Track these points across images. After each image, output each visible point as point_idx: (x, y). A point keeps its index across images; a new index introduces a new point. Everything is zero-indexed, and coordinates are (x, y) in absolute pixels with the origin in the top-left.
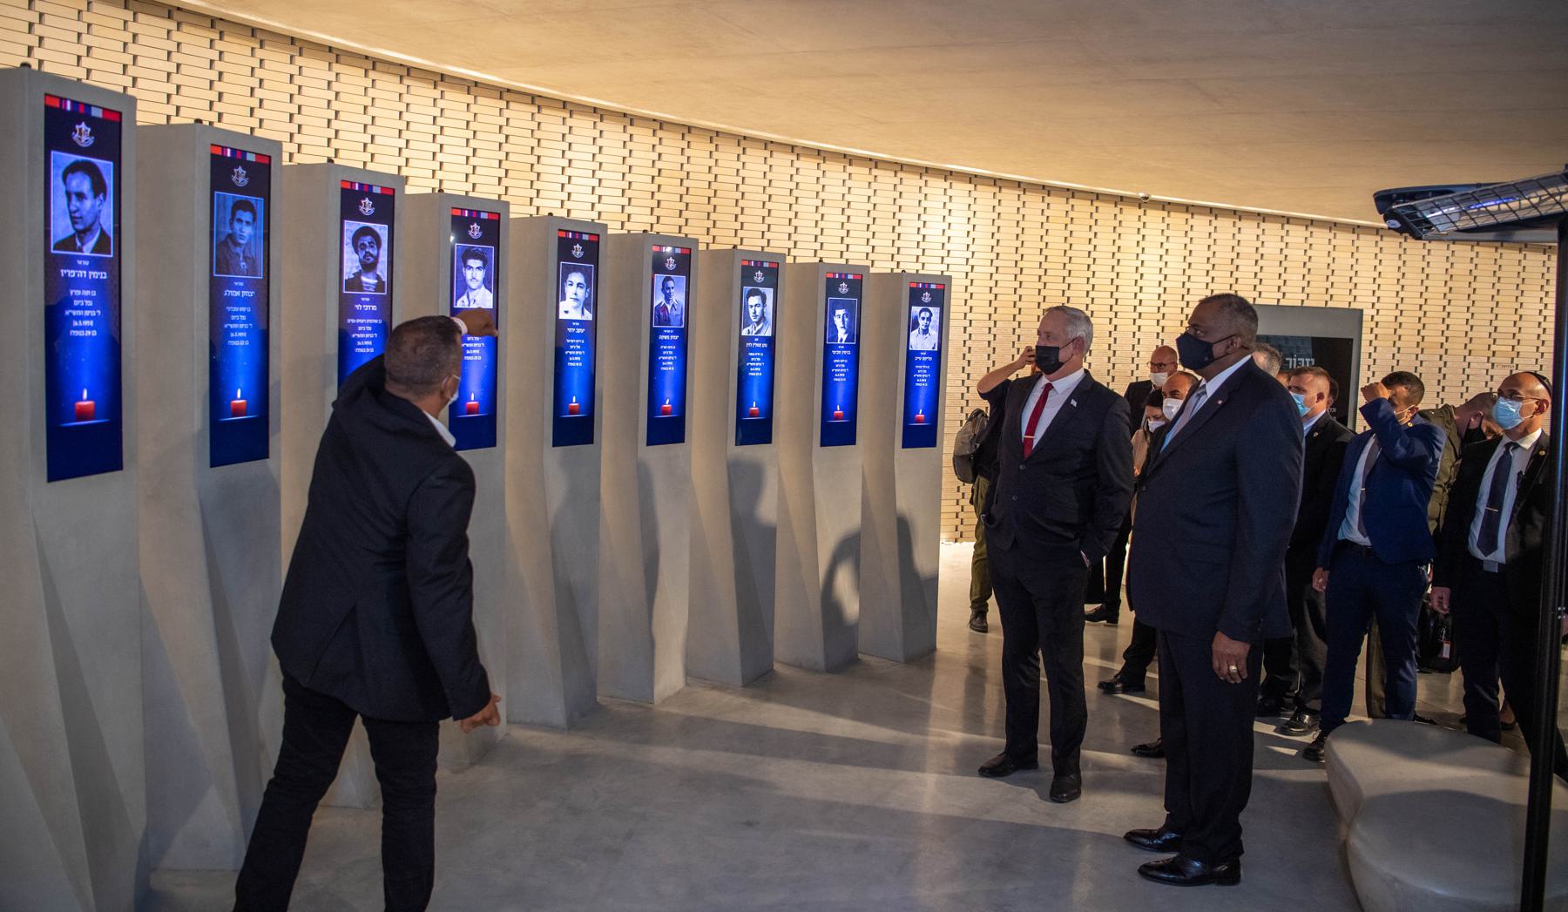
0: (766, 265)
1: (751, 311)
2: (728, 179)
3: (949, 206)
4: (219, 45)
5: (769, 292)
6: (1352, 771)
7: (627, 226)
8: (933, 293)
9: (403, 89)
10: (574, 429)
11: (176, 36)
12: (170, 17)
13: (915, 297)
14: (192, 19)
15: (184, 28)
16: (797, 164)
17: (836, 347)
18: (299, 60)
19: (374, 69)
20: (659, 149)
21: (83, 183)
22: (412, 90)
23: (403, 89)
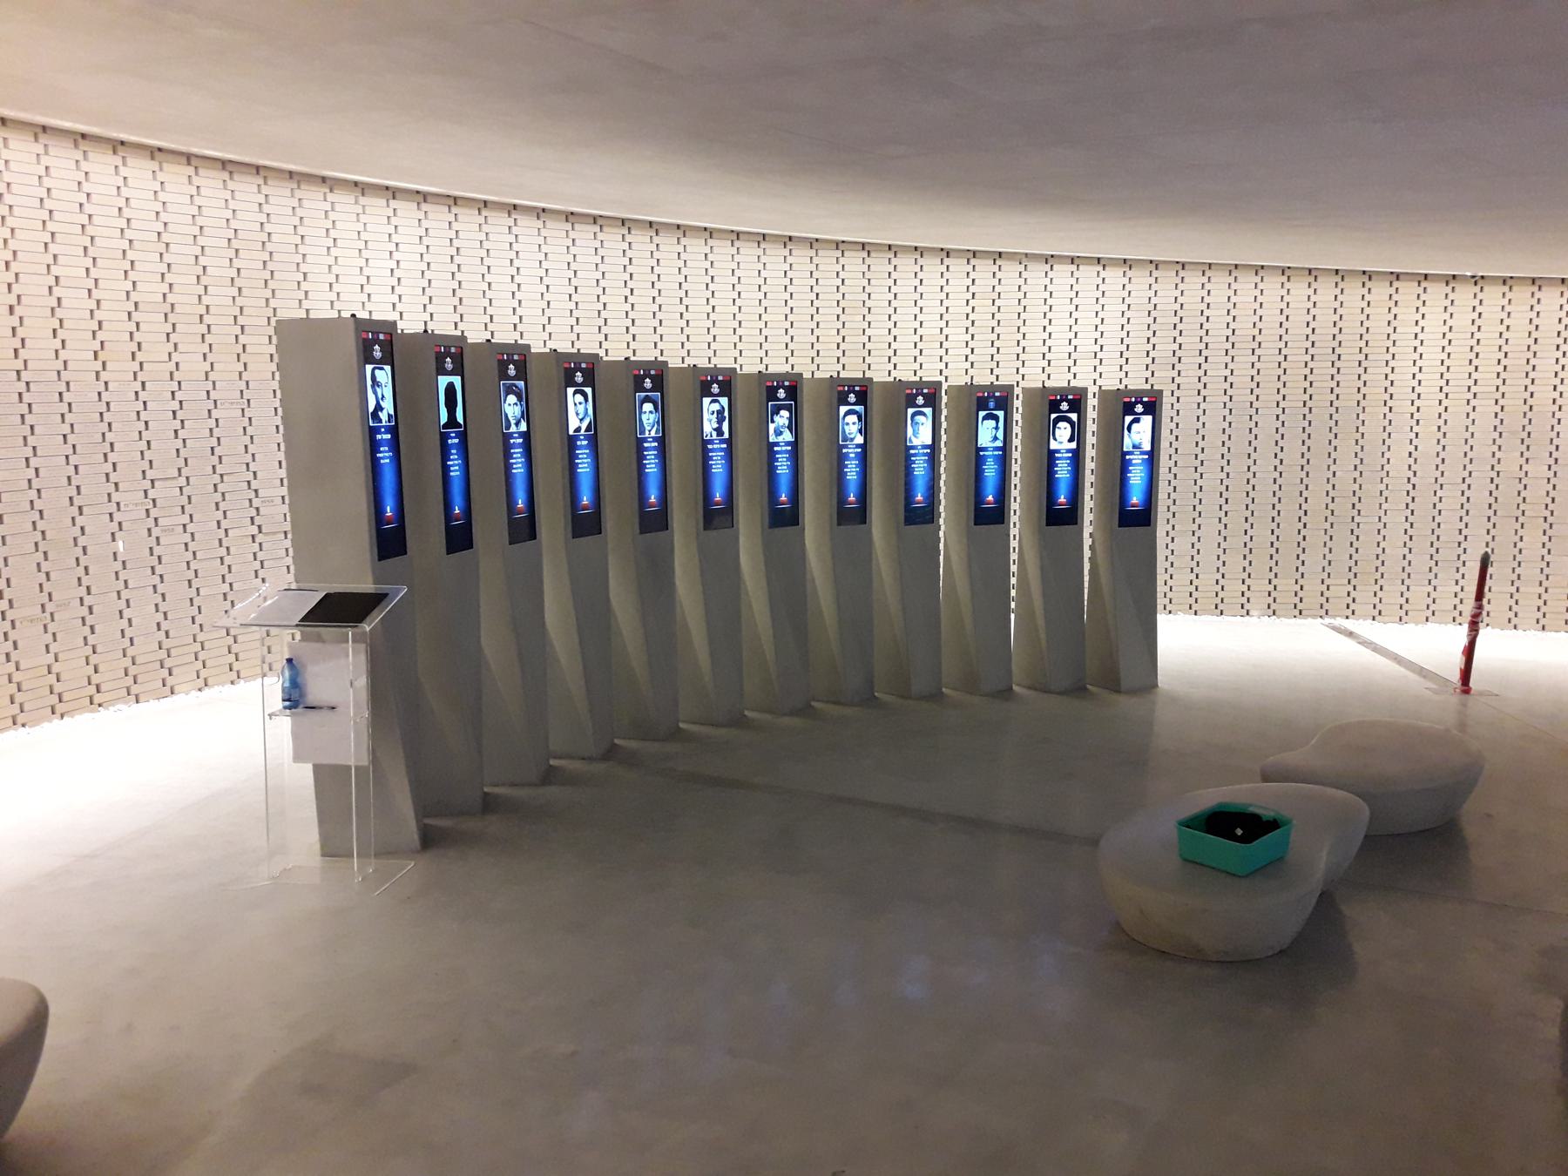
0: (381, 337)
1: (644, 417)
2: (65, 200)
3: (920, 275)
4: (629, 238)
5: (588, 390)
6: (1226, 805)
7: (894, 374)
8: (1144, 404)
9: (760, 252)
10: (459, 538)
11: (600, 236)
12: (189, 164)
13: (982, 404)
14: (170, 157)
15: (236, 176)
16: (1103, 274)
17: (645, 440)
18: (684, 241)
19: (46, 153)
20: (455, 226)
21: (579, 398)
22: (430, 215)
23: (760, 252)
